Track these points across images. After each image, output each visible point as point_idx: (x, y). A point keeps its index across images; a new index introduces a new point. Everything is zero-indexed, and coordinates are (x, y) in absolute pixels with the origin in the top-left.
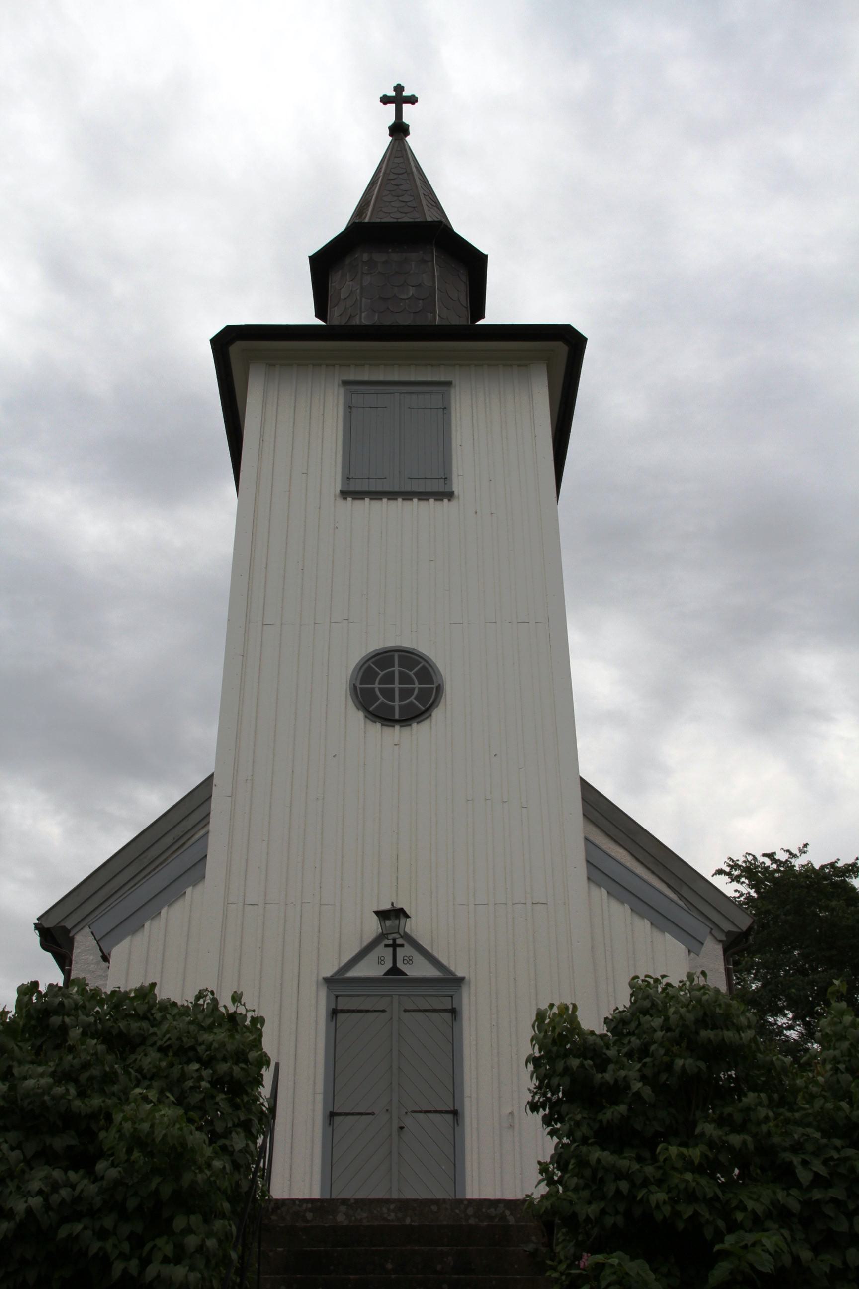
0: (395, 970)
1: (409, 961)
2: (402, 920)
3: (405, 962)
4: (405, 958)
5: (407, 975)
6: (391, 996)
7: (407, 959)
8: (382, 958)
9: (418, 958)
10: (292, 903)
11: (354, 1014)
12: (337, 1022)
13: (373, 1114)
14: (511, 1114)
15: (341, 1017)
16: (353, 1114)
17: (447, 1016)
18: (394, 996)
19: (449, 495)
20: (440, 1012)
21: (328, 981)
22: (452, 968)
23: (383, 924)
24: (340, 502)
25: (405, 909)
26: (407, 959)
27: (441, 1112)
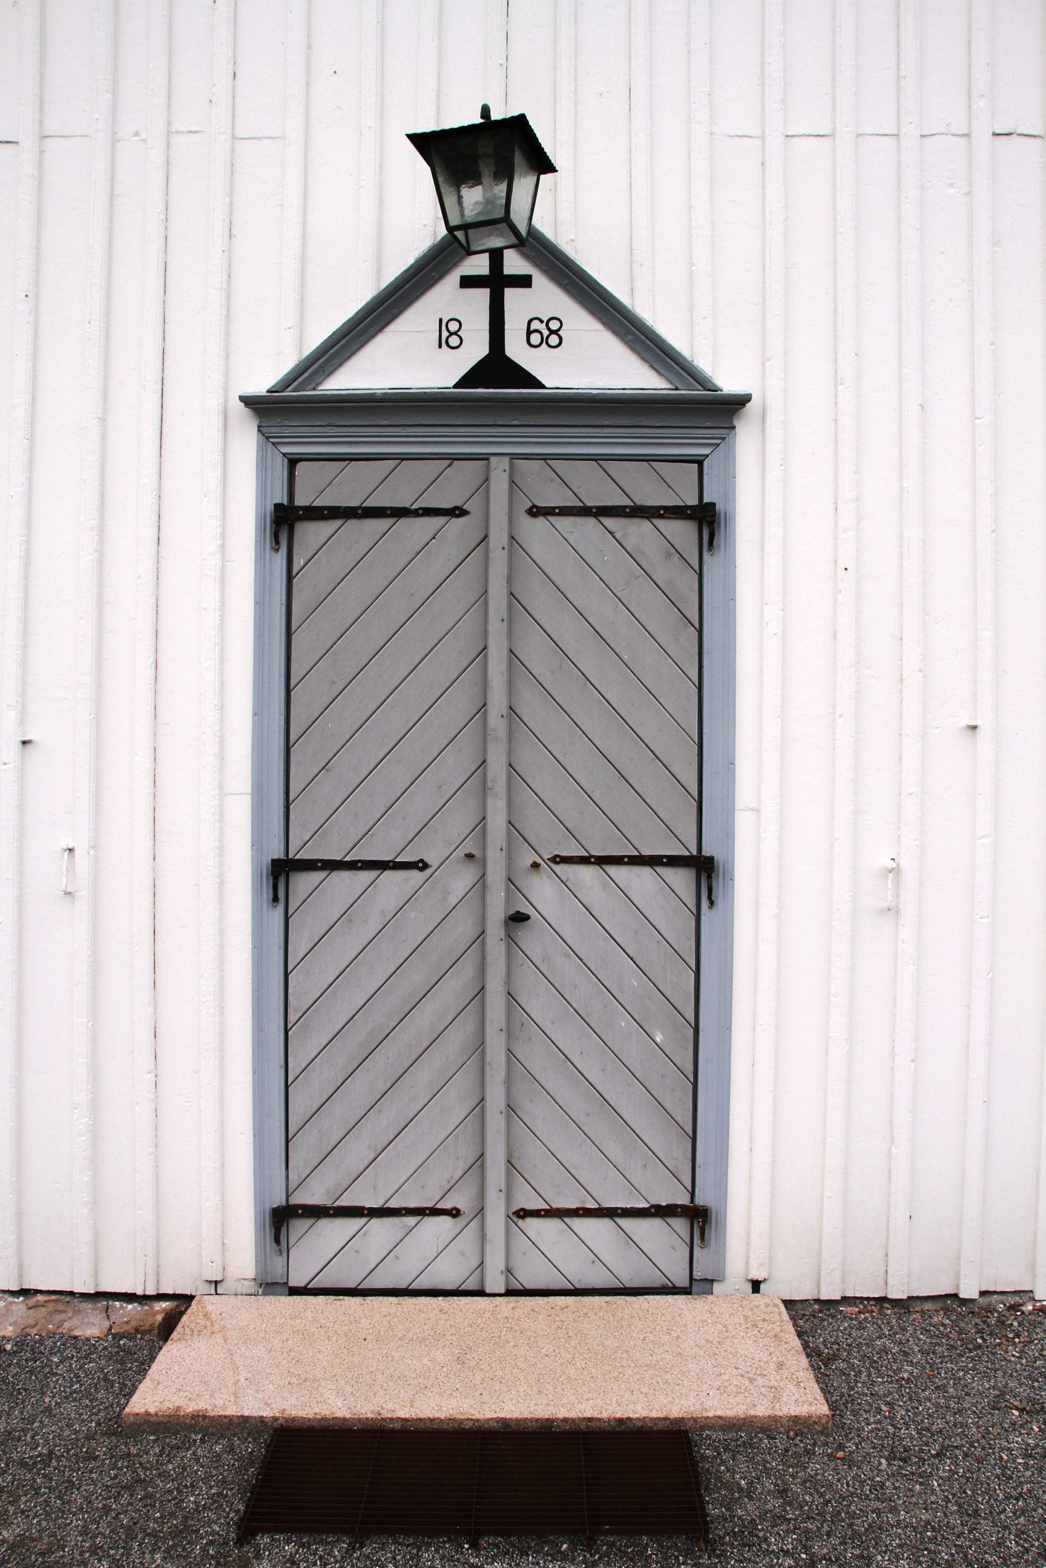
2: (523, 185)
3: (535, 339)
4: (535, 325)
5: (540, 385)
6: (485, 458)
7: (542, 327)
8: (454, 326)
10: (136, 134)
11: (352, 523)
12: (295, 551)
13: (421, 865)
14: (895, 871)
15: (310, 534)
16: (353, 866)
17: (682, 532)
18: (493, 459)
20: (661, 517)
22: (703, 363)
23: (450, 201)
24: (471, 511)
25: (532, 123)
26: (542, 327)
27: (653, 861)
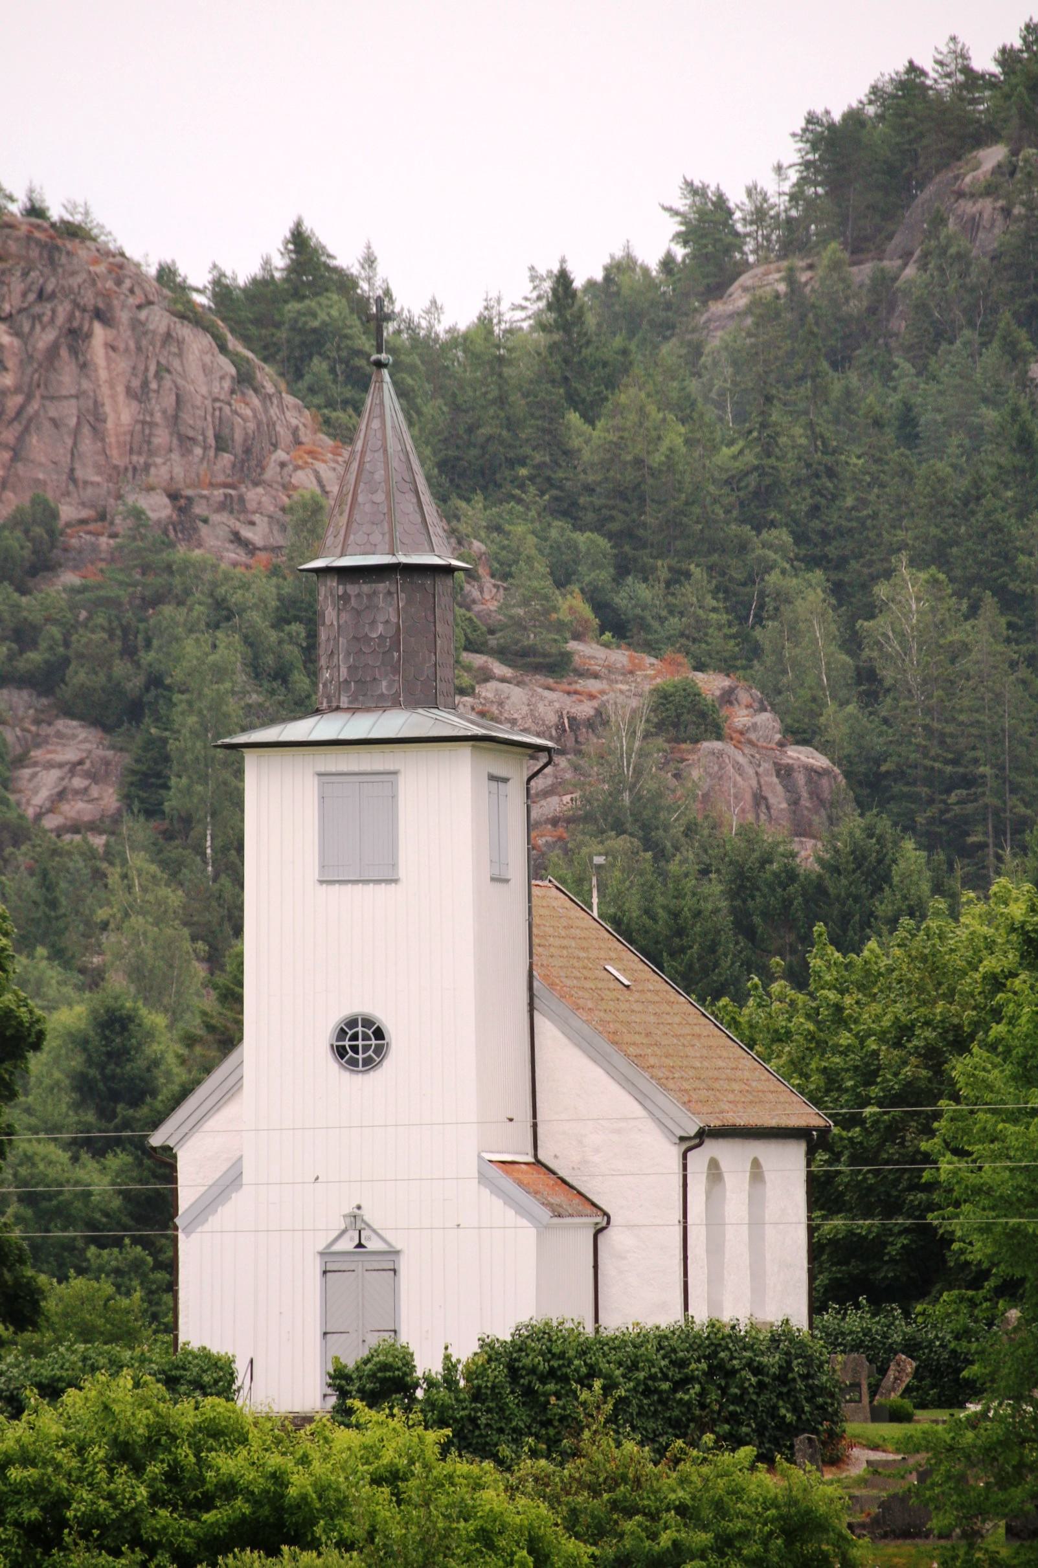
0: (360, 1245)
1: (369, 1239)
9: (374, 1237)
19: (396, 881)
21: (322, 1254)
